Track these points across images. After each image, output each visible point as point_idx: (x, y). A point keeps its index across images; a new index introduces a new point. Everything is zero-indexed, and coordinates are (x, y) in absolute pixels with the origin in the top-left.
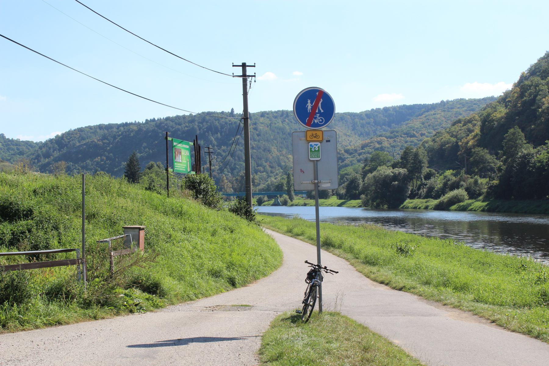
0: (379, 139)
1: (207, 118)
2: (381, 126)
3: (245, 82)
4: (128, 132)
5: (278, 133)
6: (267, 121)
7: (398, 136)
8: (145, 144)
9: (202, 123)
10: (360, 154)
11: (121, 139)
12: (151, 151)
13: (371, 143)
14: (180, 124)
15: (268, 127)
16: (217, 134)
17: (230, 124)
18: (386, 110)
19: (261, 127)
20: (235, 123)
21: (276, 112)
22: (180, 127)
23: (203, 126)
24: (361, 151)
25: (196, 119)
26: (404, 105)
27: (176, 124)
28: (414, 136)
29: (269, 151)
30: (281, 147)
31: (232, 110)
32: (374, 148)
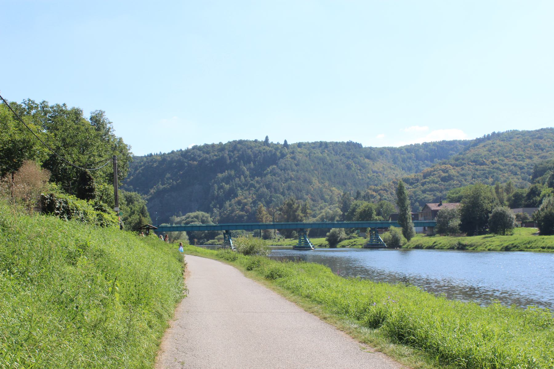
0: (443, 167)
1: (239, 146)
2: (423, 161)
4: (151, 162)
5: (318, 163)
6: (306, 151)
7: (465, 164)
8: (168, 175)
9: (233, 152)
10: (423, 184)
11: (143, 170)
12: (175, 183)
13: (434, 171)
14: (208, 153)
15: (306, 156)
16: (250, 163)
17: (264, 153)
18: (426, 145)
19: (299, 157)
20: (270, 151)
22: (208, 156)
23: (234, 155)
24: (424, 180)
25: (226, 147)
26: (444, 141)
27: (204, 153)
28: (483, 164)
29: (309, 182)
30: (323, 179)
31: (267, 138)
32: (439, 177)
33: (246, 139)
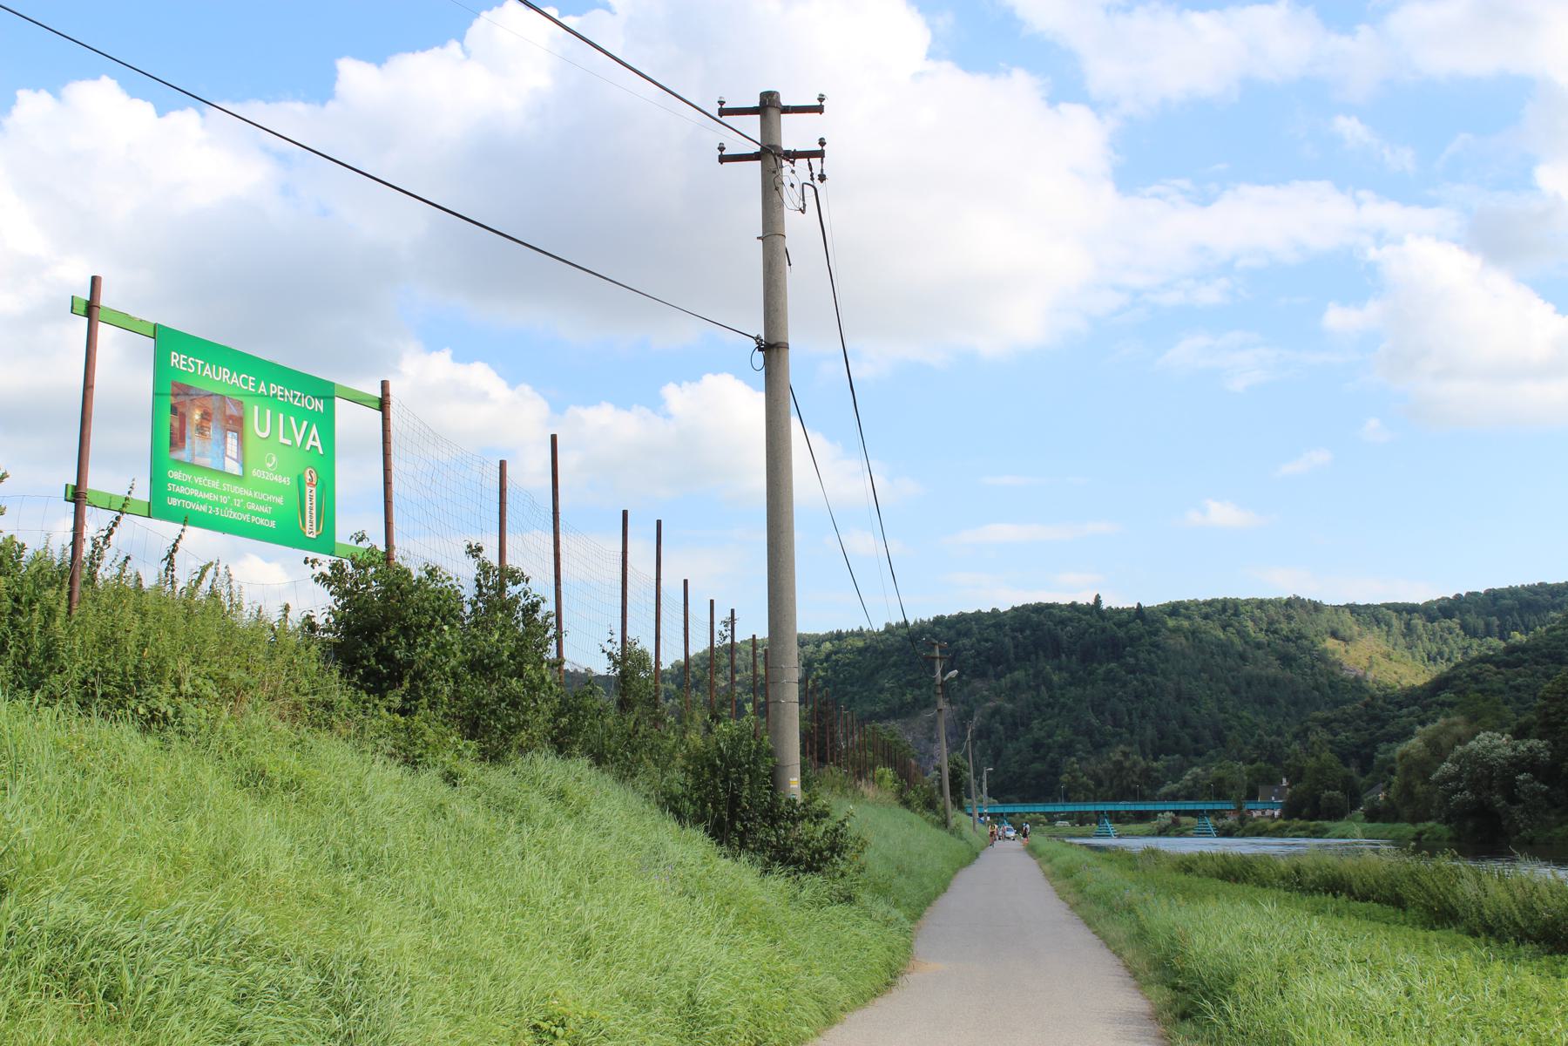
3: (771, 189)
21: (1206, 603)
31: (1098, 597)
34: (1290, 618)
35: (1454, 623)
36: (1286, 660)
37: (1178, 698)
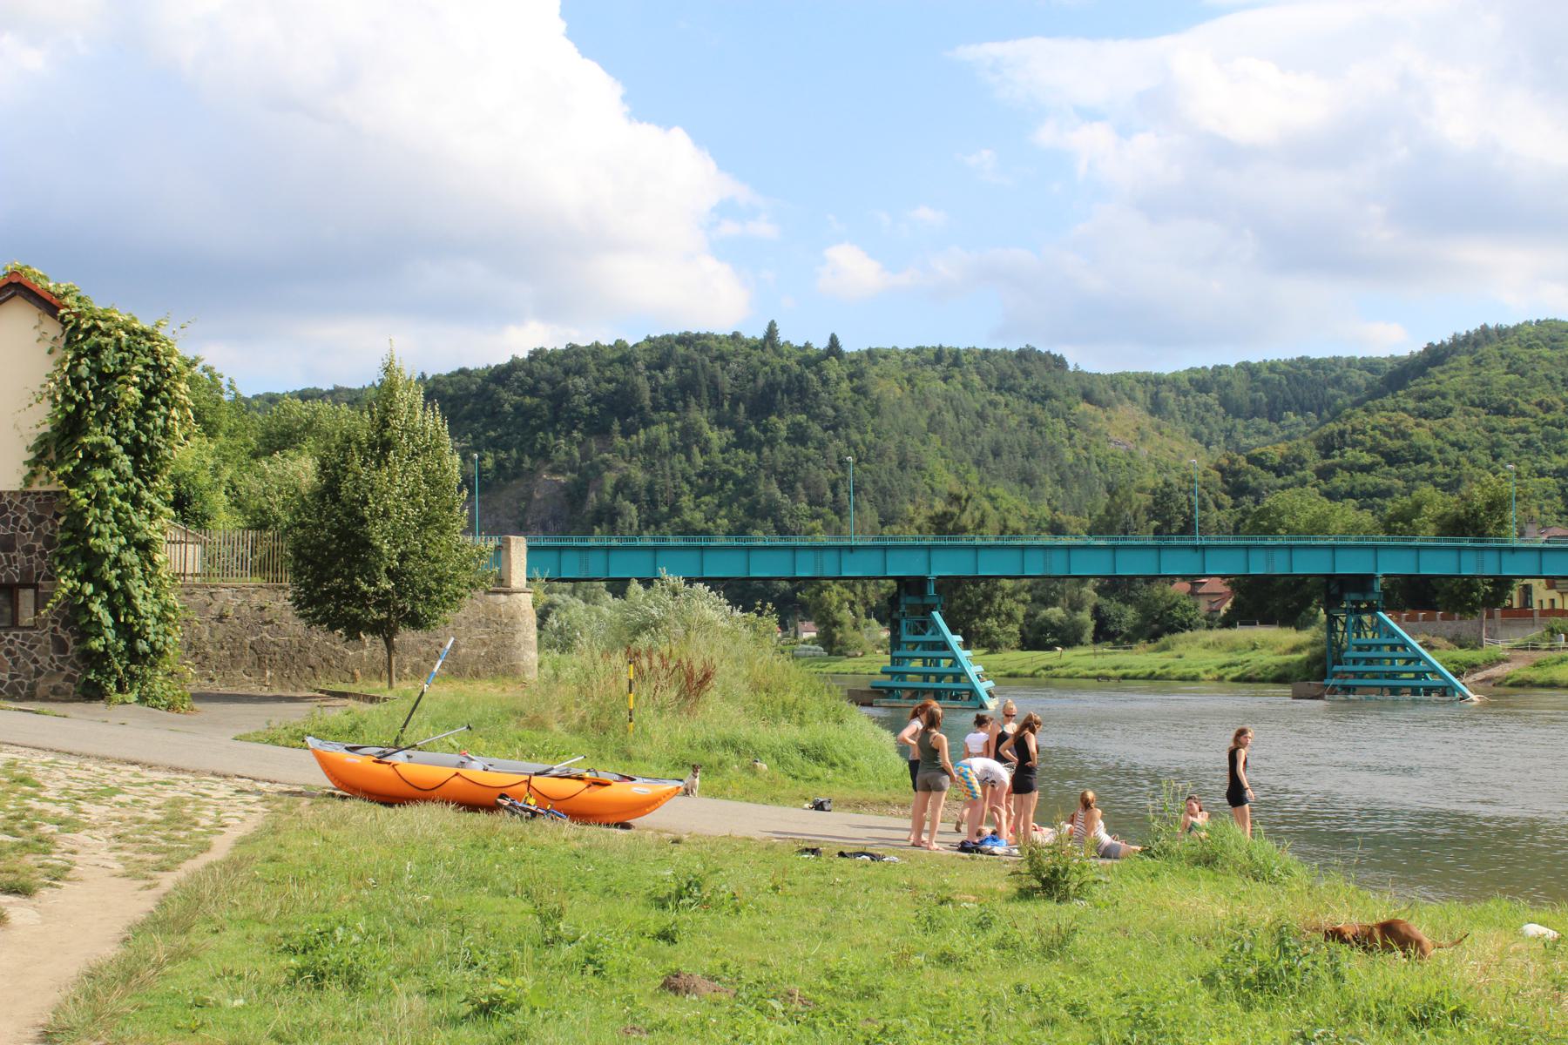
18: (1249, 370)
31: (772, 325)
33: (703, 332)
34: (1027, 374)
35: (1212, 399)
36: (1371, 371)
37: (902, 465)
